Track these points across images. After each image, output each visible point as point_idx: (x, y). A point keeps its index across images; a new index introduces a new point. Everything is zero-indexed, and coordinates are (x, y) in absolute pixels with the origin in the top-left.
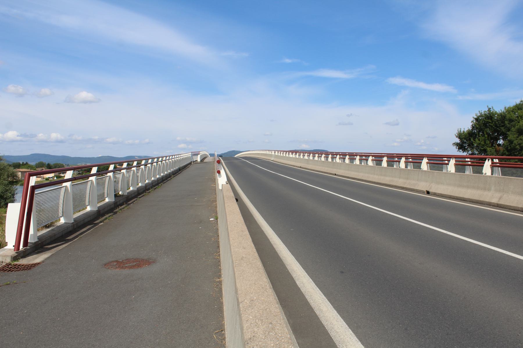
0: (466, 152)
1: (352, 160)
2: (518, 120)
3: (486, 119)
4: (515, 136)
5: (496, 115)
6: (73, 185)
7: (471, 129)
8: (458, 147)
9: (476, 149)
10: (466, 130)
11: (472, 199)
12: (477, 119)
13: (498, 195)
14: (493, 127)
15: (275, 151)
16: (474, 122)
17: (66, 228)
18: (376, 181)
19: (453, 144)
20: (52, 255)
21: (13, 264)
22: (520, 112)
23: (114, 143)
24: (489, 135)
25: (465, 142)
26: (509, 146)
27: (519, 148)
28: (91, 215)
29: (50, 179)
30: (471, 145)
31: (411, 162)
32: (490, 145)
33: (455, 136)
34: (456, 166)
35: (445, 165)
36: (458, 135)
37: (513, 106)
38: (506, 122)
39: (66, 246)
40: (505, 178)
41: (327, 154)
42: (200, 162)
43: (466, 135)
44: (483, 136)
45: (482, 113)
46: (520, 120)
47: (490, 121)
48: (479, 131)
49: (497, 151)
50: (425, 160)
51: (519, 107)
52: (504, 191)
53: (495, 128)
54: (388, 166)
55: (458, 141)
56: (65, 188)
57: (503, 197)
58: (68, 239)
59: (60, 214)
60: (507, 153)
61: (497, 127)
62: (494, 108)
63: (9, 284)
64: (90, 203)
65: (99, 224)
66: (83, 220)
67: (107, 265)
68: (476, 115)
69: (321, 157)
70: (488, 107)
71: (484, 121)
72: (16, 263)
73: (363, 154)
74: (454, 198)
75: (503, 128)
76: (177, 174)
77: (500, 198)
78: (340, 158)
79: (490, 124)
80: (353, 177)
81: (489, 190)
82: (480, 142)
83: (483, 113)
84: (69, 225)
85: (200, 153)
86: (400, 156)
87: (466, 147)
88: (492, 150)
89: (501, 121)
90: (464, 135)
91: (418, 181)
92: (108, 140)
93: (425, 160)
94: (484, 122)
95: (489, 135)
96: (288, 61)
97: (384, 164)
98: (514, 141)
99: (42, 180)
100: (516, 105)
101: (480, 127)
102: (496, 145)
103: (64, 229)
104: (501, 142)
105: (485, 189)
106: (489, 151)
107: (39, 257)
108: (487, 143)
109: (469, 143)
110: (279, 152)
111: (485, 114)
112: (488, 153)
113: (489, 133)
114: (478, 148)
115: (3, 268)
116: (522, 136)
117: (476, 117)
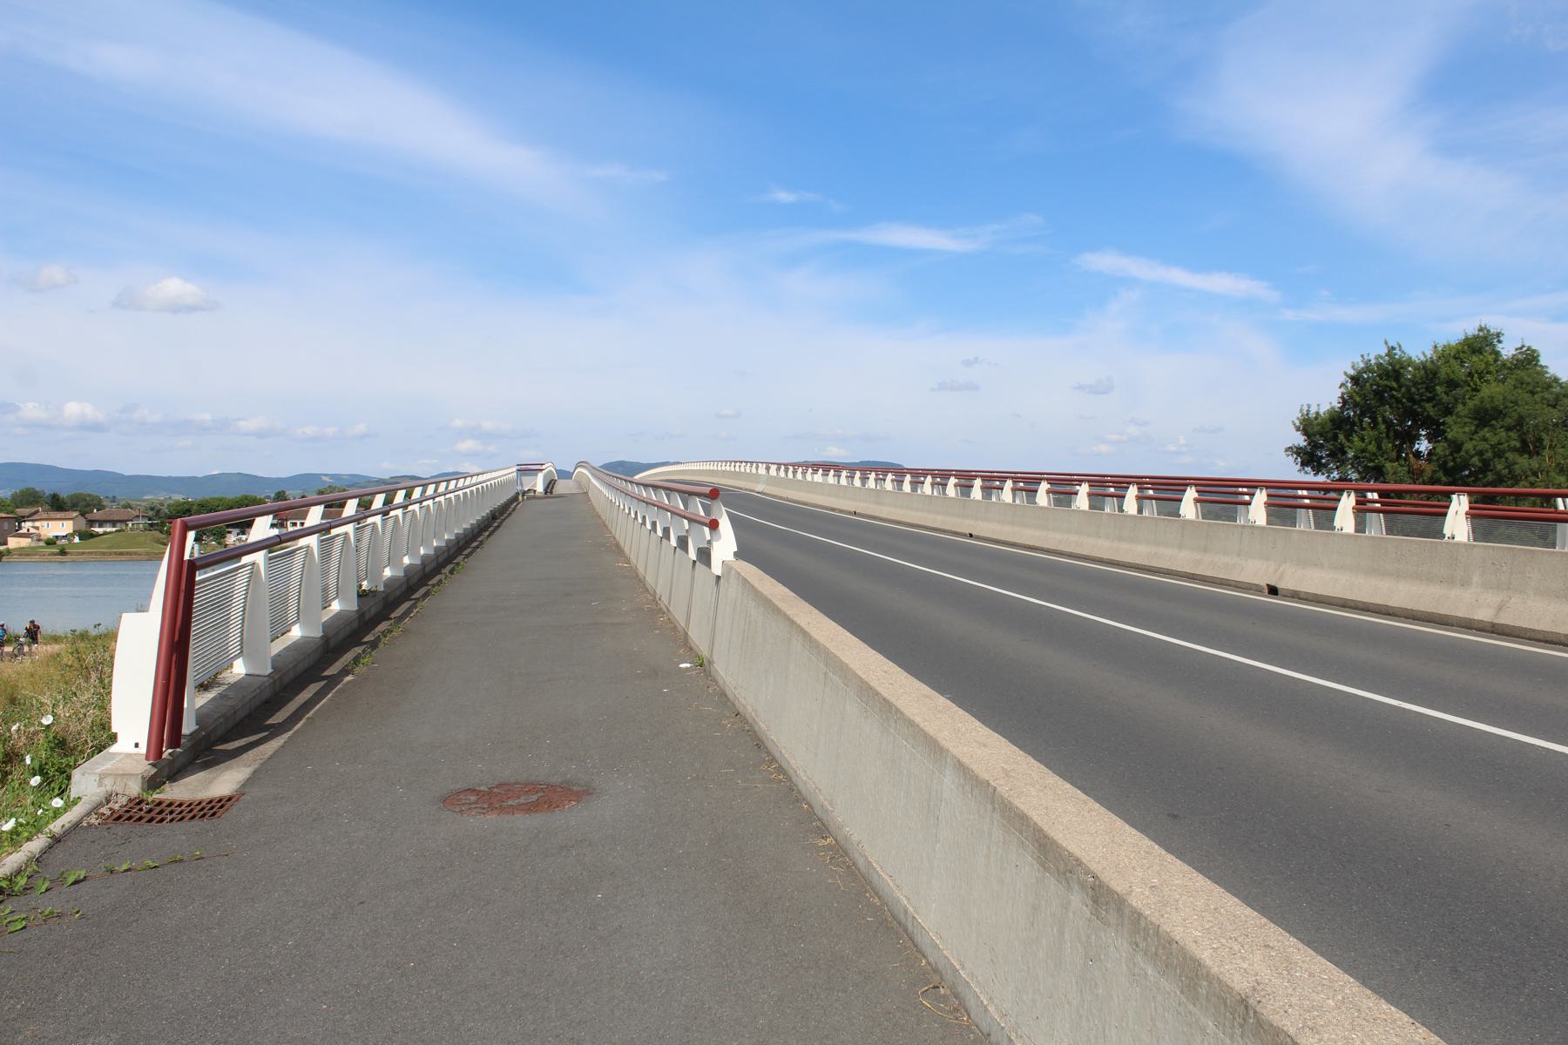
0: (1323, 474)
1: (966, 488)
2: (1472, 384)
3: (1381, 379)
4: (1467, 429)
5: (1410, 369)
6: (270, 559)
7: (1340, 408)
8: (1299, 460)
9: (1353, 467)
10: (1324, 409)
11: (1412, 610)
12: (1355, 380)
13: (1492, 598)
14: (1403, 404)
15: (777, 464)
16: (1347, 387)
17: (258, 691)
18: (1106, 556)
19: (1287, 450)
20: (255, 772)
21: (150, 799)
22: (1477, 359)
23: (261, 435)
24: (1389, 424)
25: (1322, 446)
26: (1451, 457)
27: (1480, 464)
28: (309, 652)
29: (58, 542)
30: (1338, 454)
31: (1151, 498)
32: (1394, 454)
33: (1293, 427)
34: (1477, 521)
35: (1303, 510)
36: (1301, 423)
37: (1457, 342)
38: (1438, 387)
39: (282, 747)
40: (1515, 548)
41: (900, 472)
42: (543, 495)
43: (1326, 423)
44: (1372, 428)
45: (1370, 361)
46: (1478, 383)
47: (1394, 385)
48: (1363, 414)
49: (1413, 473)
50: (1191, 494)
51: (1475, 345)
52: (1509, 588)
53: (1409, 404)
54: (1091, 507)
55: (1300, 440)
56: (250, 567)
57: (1509, 606)
58: (274, 724)
59: (234, 647)
60: (1444, 479)
61: (1414, 402)
62: (1403, 348)
63: (181, 861)
64: (301, 614)
65: (343, 680)
66: (295, 666)
67: (451, 800)
68: (1353, 367)
69: (1002, 489)
70: (1386, 343)
71: (1378, 385)
72: (157, 796)
73: (995, 474)
74: (1344, 606)
75: (1431, 404)
76: (491, 529)
77: (1500, 609)
78: (933, 485)
79: (1395, 393)
80: (1031, 543)
81: (1465, 583)
82: (1364, 445)
83: (1373, 362)
84: (264, 683)
85: (544, 467)
86: (1122, 483)
87: (1324, 461)
88: (1400, 469)
89: (1424, 386)
90: (1318, 425)
91: (1239, 555)
92: (242, 424)
93: (1191, 494)
94: (1375, 387)
95: (1389, 424)
96: (784, 197)
97: (1082, 500)
98: (1463, 444)
99: (33, 545)
100: (1467, 339)
101: (1364, 402)
102: (1411, 456)
103: (254, 694)
104: (1423, 446)
105: (1450, 581)
106: (1391, 471)
107: (215, 778)
108: (1384, 448)
109: (1332, 447)
110: (791, 468)
111: (1379, 365)
112: (1389, 477)
113: (1391, 420)
114: (1359, 463)
115: (127, 811)
116: (1486, 429)
117: (1352, 372)
